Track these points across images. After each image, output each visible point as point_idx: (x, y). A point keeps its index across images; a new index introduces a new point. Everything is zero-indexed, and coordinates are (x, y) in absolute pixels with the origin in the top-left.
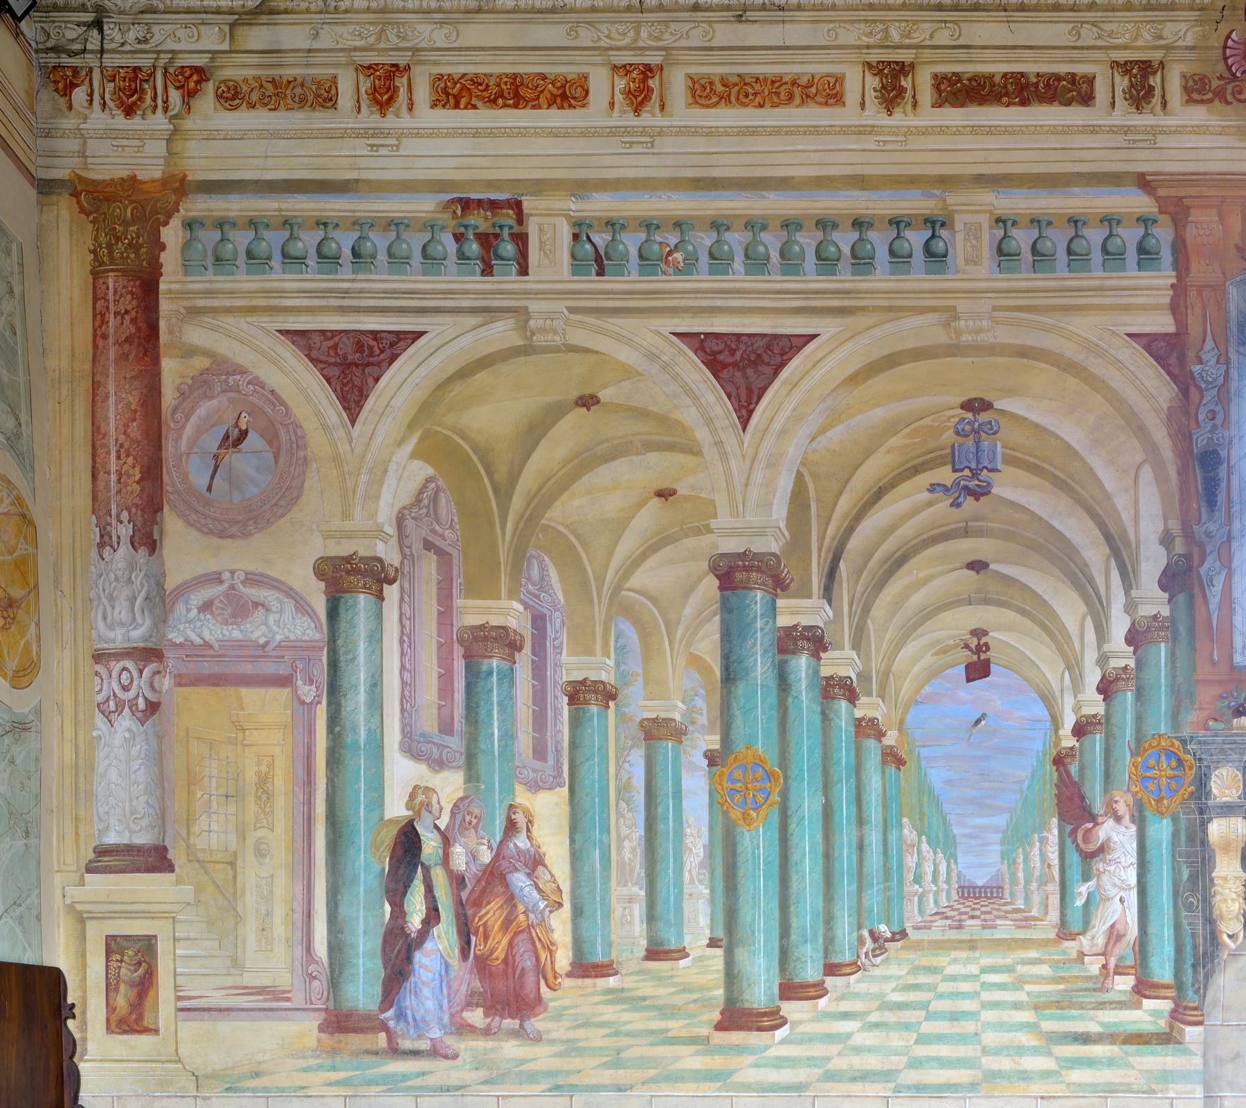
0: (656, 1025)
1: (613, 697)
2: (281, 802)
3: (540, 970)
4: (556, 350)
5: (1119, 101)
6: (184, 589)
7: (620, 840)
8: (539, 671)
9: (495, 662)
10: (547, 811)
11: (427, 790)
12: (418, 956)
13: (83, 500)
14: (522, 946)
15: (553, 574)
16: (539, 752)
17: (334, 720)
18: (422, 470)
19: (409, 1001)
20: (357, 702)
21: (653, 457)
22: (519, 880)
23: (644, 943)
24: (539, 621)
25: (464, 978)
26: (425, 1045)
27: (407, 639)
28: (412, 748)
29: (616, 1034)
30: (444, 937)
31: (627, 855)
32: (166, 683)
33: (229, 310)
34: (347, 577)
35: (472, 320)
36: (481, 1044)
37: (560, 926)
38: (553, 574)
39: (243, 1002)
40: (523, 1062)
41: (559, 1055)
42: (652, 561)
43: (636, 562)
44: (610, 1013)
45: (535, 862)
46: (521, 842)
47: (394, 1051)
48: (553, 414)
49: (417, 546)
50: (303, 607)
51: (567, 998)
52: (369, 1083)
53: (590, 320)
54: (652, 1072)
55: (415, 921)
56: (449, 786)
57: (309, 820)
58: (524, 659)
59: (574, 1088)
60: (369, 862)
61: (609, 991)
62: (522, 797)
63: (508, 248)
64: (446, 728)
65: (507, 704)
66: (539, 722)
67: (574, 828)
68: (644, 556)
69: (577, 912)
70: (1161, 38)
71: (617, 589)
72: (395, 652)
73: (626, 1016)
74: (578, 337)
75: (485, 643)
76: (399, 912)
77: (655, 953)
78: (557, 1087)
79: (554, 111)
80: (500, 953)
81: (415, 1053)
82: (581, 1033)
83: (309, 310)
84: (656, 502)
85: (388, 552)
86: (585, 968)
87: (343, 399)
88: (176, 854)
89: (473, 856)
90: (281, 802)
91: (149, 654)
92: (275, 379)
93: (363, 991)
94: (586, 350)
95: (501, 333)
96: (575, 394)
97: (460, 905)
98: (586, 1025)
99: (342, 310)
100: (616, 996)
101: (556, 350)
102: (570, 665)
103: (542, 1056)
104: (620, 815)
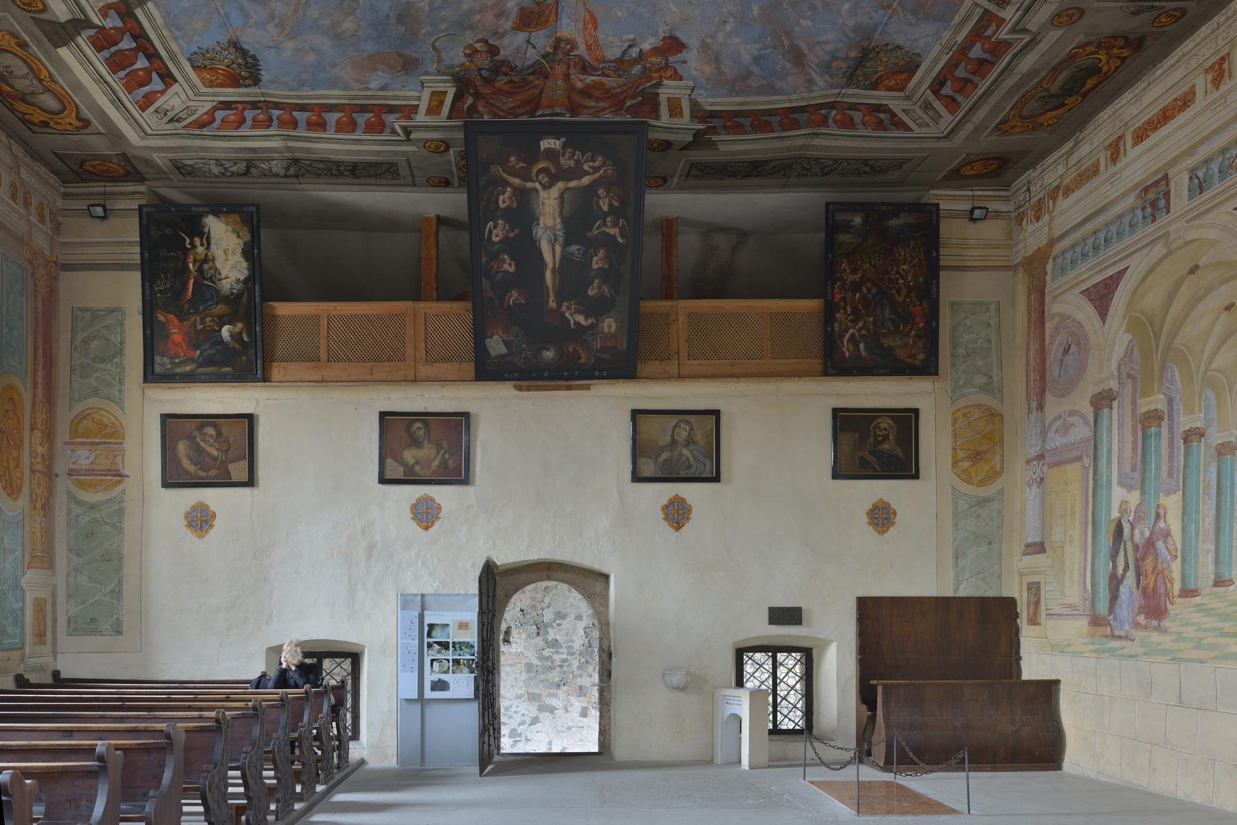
0: (1218, 625)
1: (1202, 435)
2: (1078, 516)
3: (1167, 594)
4: (1180, 248)
5: (919, 103)
6: (1051, 424)
7: (1204, 517)
8: (1171, 427)
9: (1153, 429)
10: (1172, 503)
11: (1127, 502)
12: (1121, 588)
13: (1024, 396)
14: (1160, 581)
15: (1177, 374)
16: (1170, 475)
17: (1095, 473)
18: (1128, 337)
19: (1118, 611)
20: (1103, 461)
21: (1224, 288)
22: (1160, 545)
23: (1213, 576)
24: (1170, 401)
25: (1138, 600)
26: (1123, 634)
27: (1121, 426)
28: (1122, 484)
29: (1199, 630)
30: (1131, 574)
31: (1207, 526)
32: (1046, 468)
33: (1065, 291)
34: (1102, 401)
35: (1146, 251)
36: (1143, 634)
37: (1176, 567)
38: (1177, 374)
39: (1065, 611)
40: (1160, 644)
41: (1174, 641)
42: (1222, 350)
43: (1214, 354)
44: (1197, 618)
45: (1167, 534)
46: (1161, 524)
47: (1114, 637)
48: (1179, 283)
49: (1124, 376)
50: (1086, 423)
51: (1179, 609)
52: (1104, 652)
53: (1196, 222)
54: (1216, 653)
55: (1120, 571)
56: (1134, 498)
57: (1086, 523)
58: (1165, 423)
59: (1181, 659)
60: (1106, 541)
61: (1197, 605)
62: (1163, 500)
63: (1162, 203)
64: (1134, 470)
65: (1158, 446)
66: (1171, 457)
67: (1184, 514)
68: (1219, 348)
69: (1184, 560)
70: (367, 89)
71: (1206, 371)
72: (1118, 436)
73: (1205, 620)
74: (1191, 235)
75: (1154, 417)
76: (1115, 567)
77: (1218, 583)
78: (1174, 659)
79: (1182, 114)
80: (1151, 586)
81: (1120, 637)
82: (1184, 629)
83: (1090, 277)
84: (1225, 314)
85: (1113, 384)
86: (1187, 593)
87: (1100, 315)
88: (1047, 546)
89: (1142, 534)
90: (1078, 516)
91: (1041, 457)
92: (1079, 316)
93: (1102, 607)
94: (1193, 241)
95: (1159, 250)
96: (1187, 269)
97: (1137, 560)
98: (1186, 624)
99: (1100, 271)
100: (1200, 608)
101: (1180, 248)
102: (1185, 422)
103: (1166, 641)
104: (1204, 503)
